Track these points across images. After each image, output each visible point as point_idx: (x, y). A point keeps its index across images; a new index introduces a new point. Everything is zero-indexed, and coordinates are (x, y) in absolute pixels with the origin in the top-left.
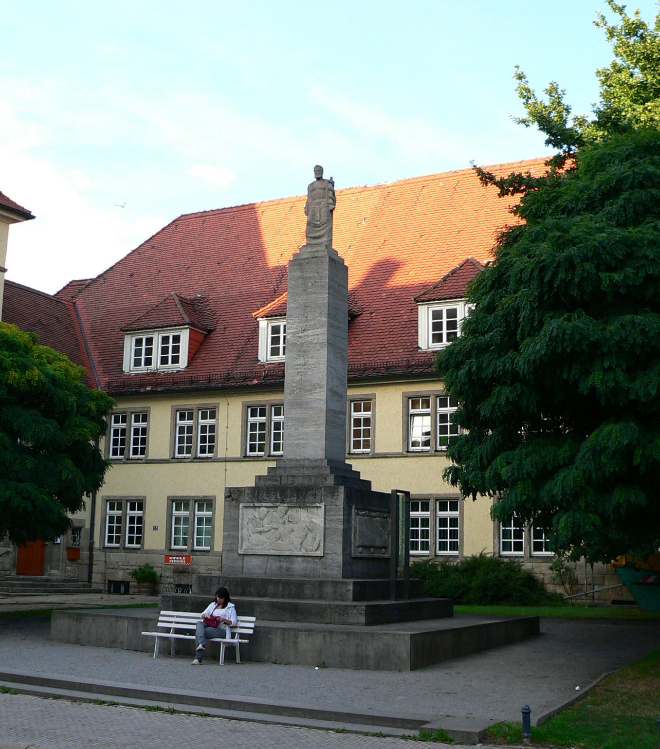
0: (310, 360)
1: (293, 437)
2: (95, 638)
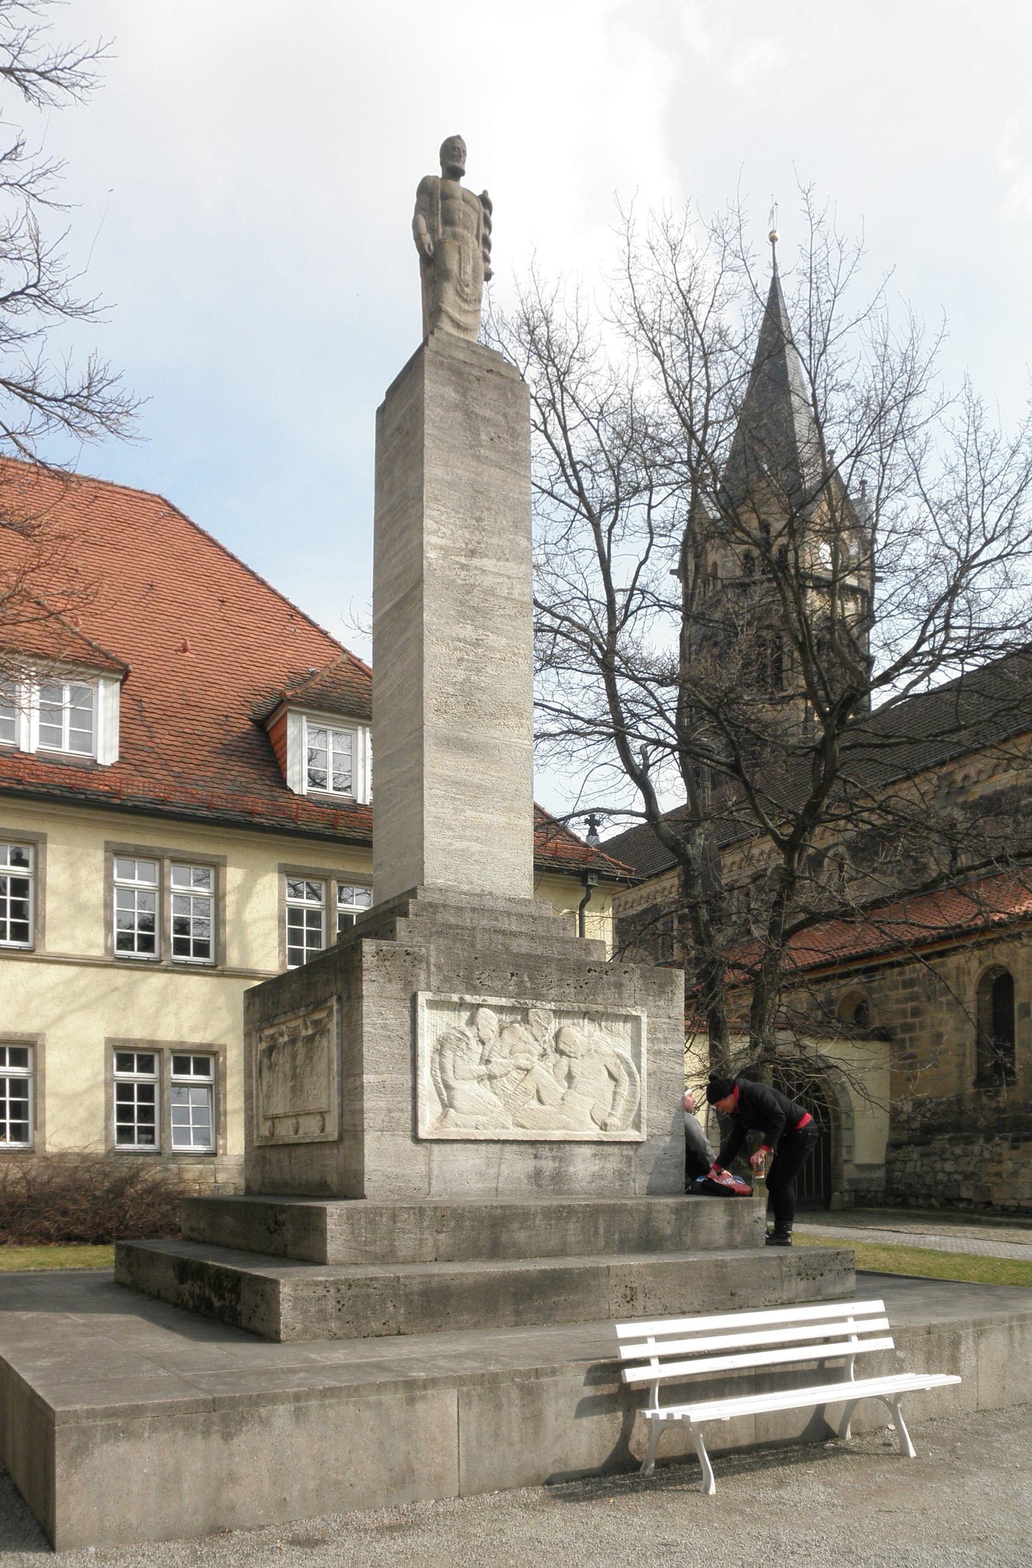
0: (492, 637)
1: (450, 828)
2: (312, 1484)
